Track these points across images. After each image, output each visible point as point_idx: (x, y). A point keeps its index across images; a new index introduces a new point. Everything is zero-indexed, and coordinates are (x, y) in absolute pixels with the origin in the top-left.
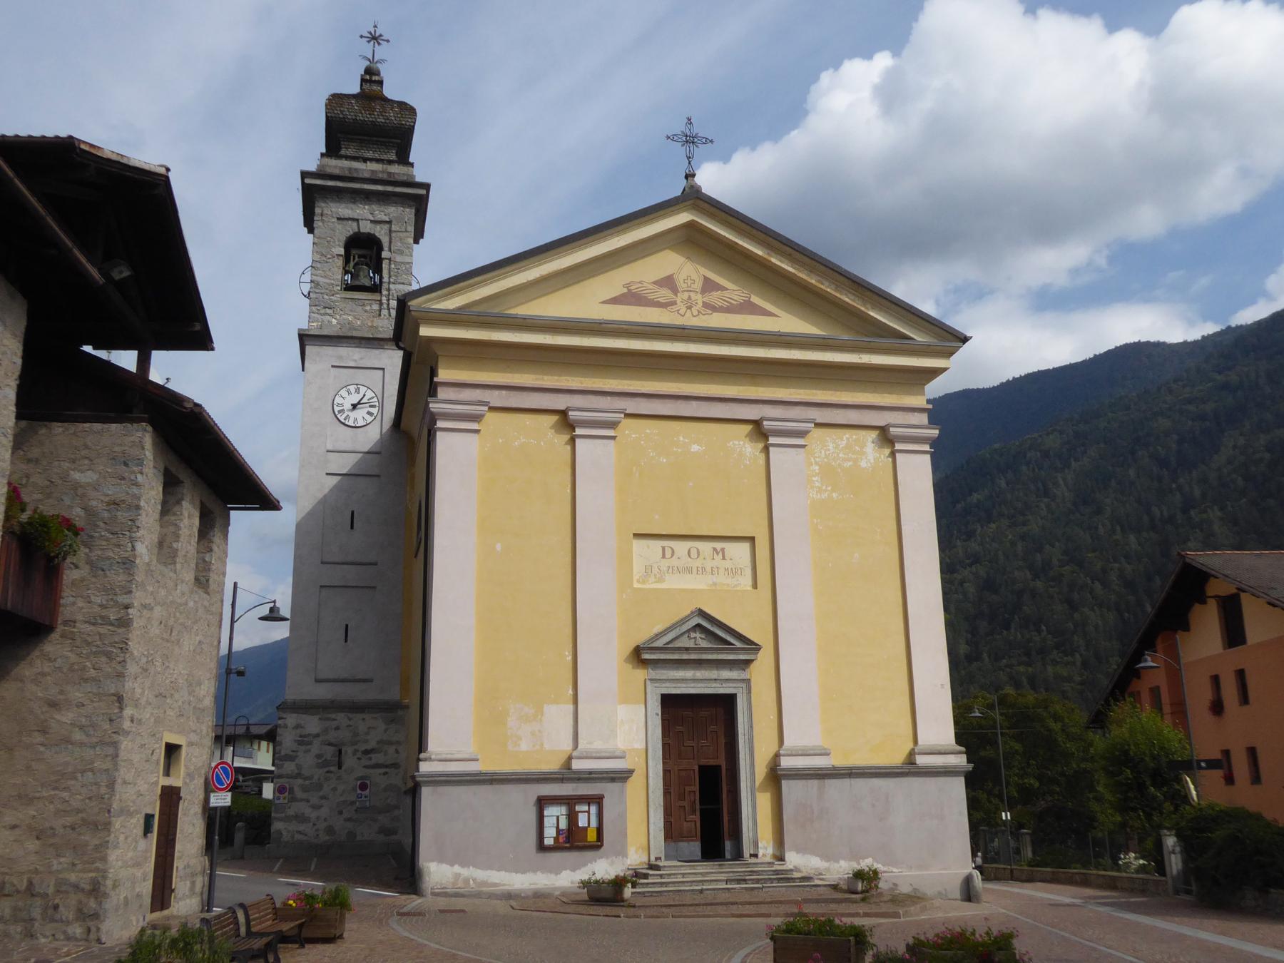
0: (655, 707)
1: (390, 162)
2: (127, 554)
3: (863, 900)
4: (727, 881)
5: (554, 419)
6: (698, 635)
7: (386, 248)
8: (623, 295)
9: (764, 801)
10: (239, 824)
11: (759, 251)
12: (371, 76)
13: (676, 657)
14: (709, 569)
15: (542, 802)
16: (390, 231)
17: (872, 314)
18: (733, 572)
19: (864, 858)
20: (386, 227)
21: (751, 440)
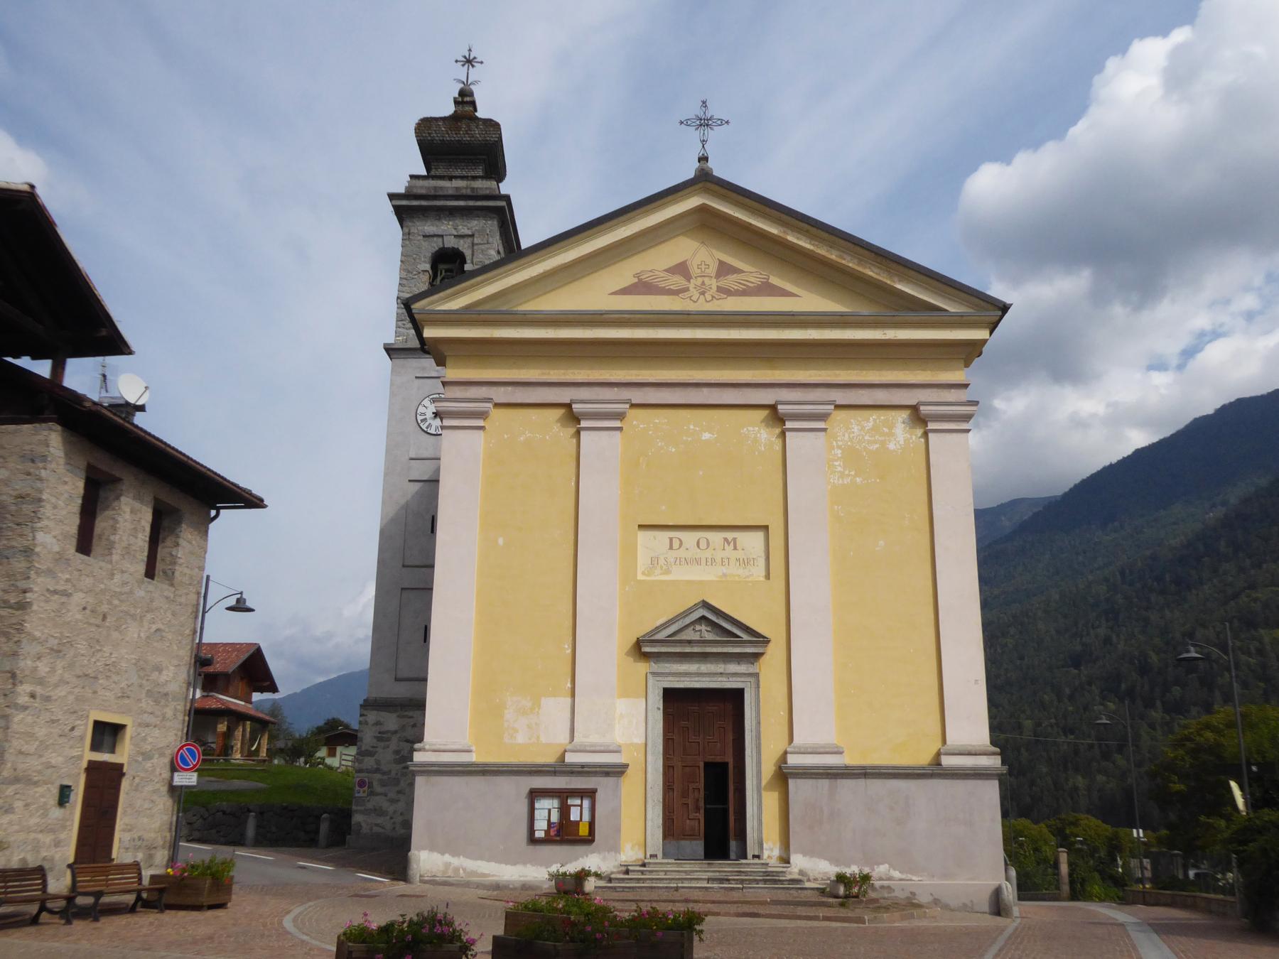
0: (657, 701)
1: (474, 178)
2: (26, 543)
3: (842, 905)
4: (708, 880)
5: (559, 412)
6: (703, 628)
7: (468, 261)
8: (634, 285)
9: (771, 801)
10: (325, 816)
11: (774, 230)
12: (465, 99)
13: (678, 650)
14: (718, 560)
15: (534, 795)
16: (473, 244)
17: (899, 286)
18: (745, 562)
19: (879, 864)
20: (469, 240)
21: (767, 426)
